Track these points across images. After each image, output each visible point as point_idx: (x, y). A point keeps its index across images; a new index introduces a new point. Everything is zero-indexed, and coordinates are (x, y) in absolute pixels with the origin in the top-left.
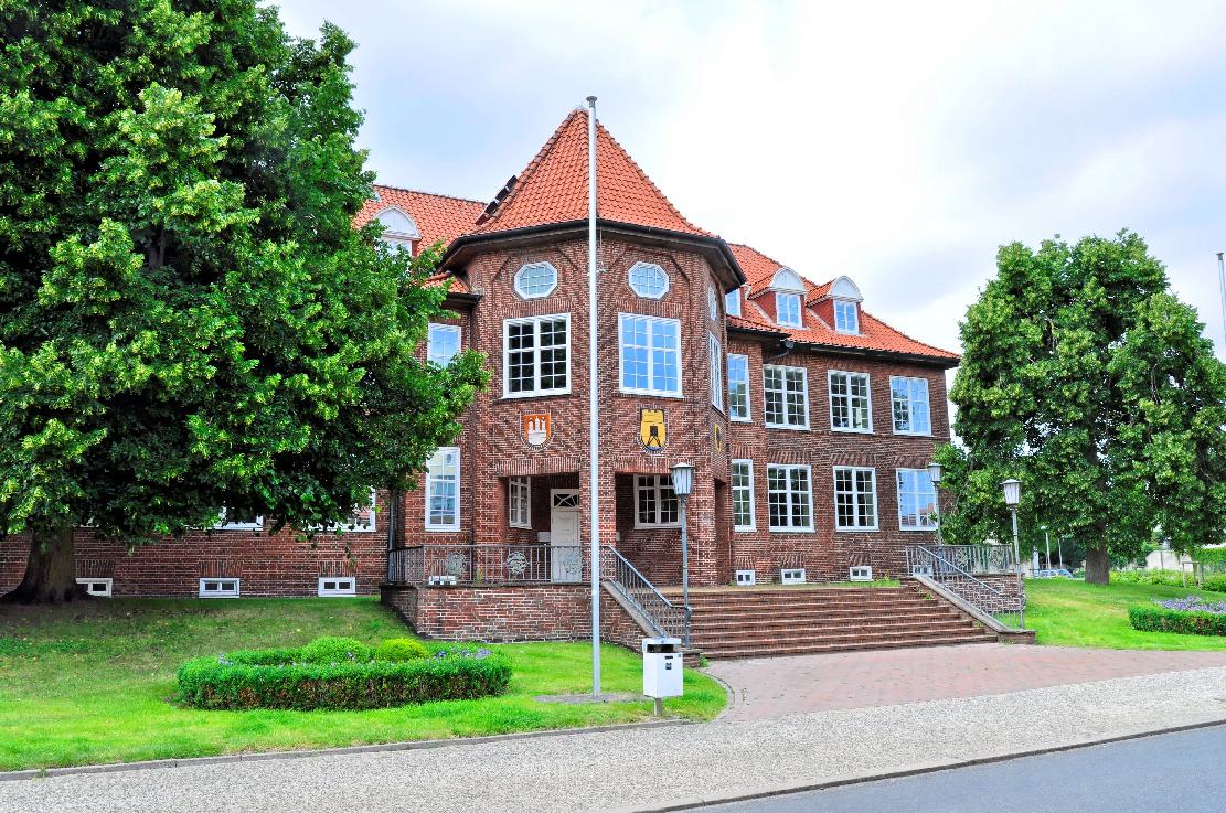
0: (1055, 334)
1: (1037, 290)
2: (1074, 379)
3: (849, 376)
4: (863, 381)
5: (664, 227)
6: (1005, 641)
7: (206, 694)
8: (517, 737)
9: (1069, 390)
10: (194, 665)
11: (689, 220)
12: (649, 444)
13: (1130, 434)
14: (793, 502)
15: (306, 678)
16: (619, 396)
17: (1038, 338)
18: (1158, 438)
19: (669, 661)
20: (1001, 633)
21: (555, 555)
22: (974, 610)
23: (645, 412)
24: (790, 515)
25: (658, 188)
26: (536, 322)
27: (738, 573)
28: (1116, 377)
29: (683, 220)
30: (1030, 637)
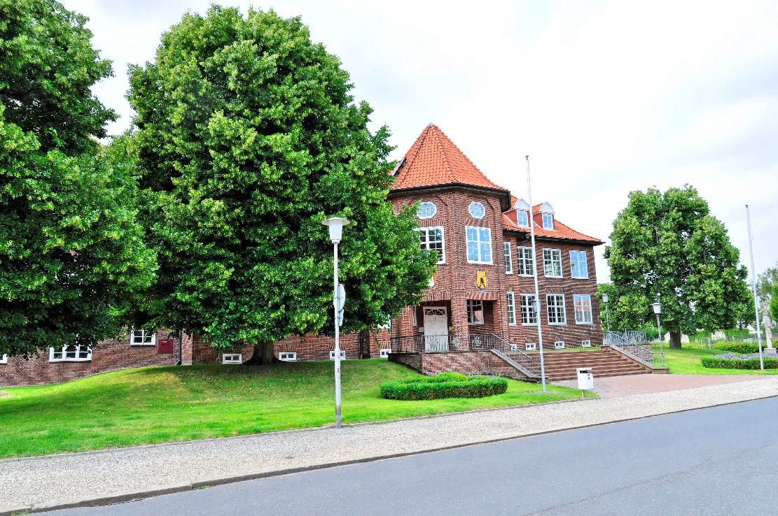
1: (649, 214)
3: (552, 250)
7: (387, 394)
10: (386, 383)
13: (694, 279)
15: (456, 387)
18: (706, 282)
29: (489, 181)
30: (667, 371)
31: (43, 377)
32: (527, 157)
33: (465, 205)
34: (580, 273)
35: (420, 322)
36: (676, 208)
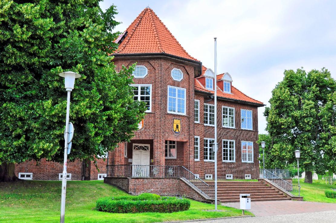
0: (302, 101)
1: (297, 86)
2: (308, 117)
3: (228, 108)
4: (233, 110)
5: (179, 56)
6: (294, 200)
8: (218, 219)
9: (306, 120)
11: (189, 54)
12: (176, 130)
14: (207, 153)
16: (168, 114)
17: (297, 103)
19: (248, 200)
20: (292, 197)
21: (133, 167)
22: (284, 190)
23: (175, 120)
24: (208, 156)
25: (178, 41)
26: (140, 86)
27: (246, 175)
28: (322, 117)
30: (301, 199)
31: (68, 144)
32: (215, 39)
33: (168, 70)
34: (247, 126)
35: (130, 155)
36: (316, 84)
